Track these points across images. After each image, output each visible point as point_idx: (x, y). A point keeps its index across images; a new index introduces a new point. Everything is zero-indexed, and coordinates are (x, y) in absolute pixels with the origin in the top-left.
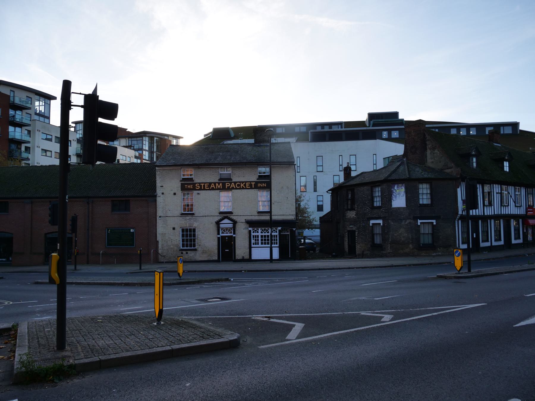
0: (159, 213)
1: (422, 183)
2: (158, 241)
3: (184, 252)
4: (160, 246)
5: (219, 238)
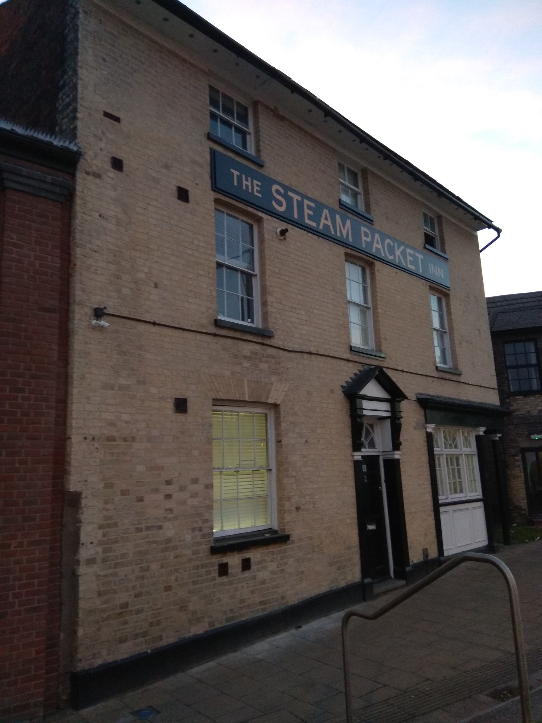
0: (92, 284)
1: (438, 500)
2: (75, 500)
3: (234, 560)
4: (89, 532)
5: (357, 464)
